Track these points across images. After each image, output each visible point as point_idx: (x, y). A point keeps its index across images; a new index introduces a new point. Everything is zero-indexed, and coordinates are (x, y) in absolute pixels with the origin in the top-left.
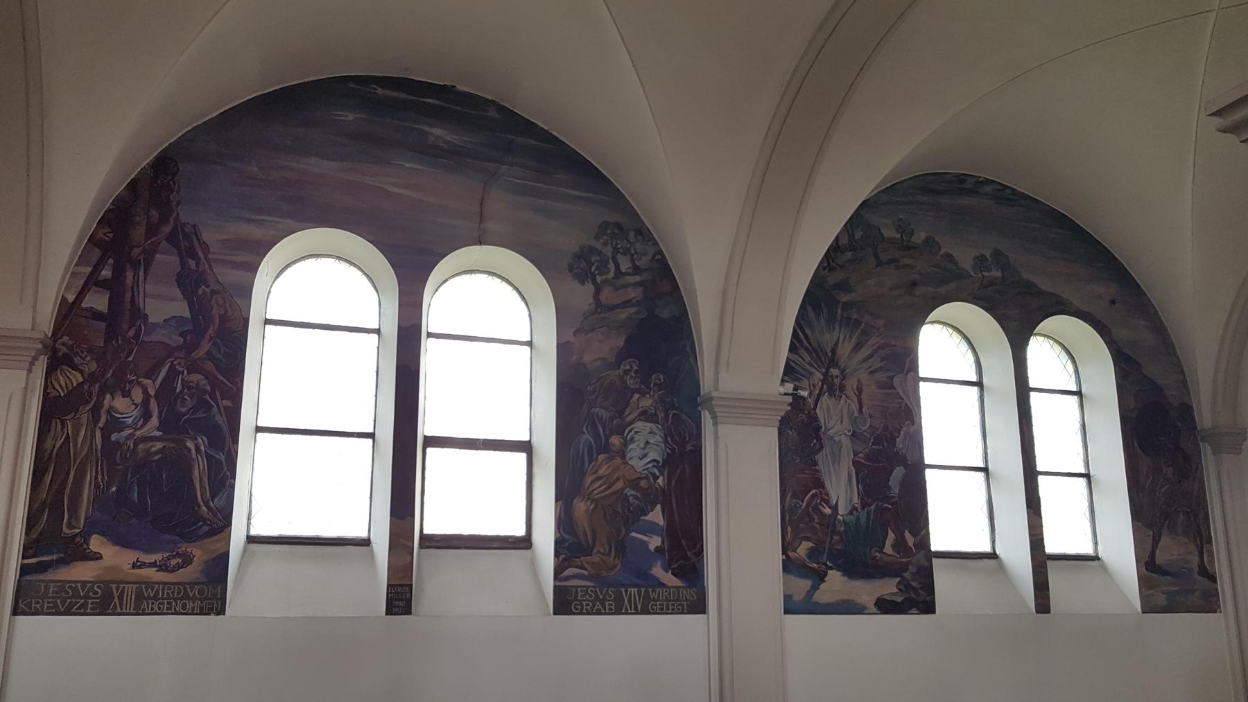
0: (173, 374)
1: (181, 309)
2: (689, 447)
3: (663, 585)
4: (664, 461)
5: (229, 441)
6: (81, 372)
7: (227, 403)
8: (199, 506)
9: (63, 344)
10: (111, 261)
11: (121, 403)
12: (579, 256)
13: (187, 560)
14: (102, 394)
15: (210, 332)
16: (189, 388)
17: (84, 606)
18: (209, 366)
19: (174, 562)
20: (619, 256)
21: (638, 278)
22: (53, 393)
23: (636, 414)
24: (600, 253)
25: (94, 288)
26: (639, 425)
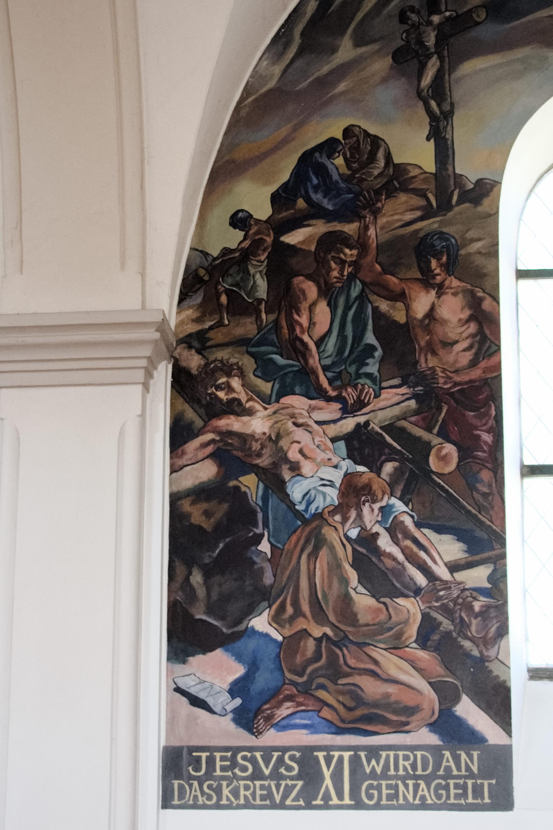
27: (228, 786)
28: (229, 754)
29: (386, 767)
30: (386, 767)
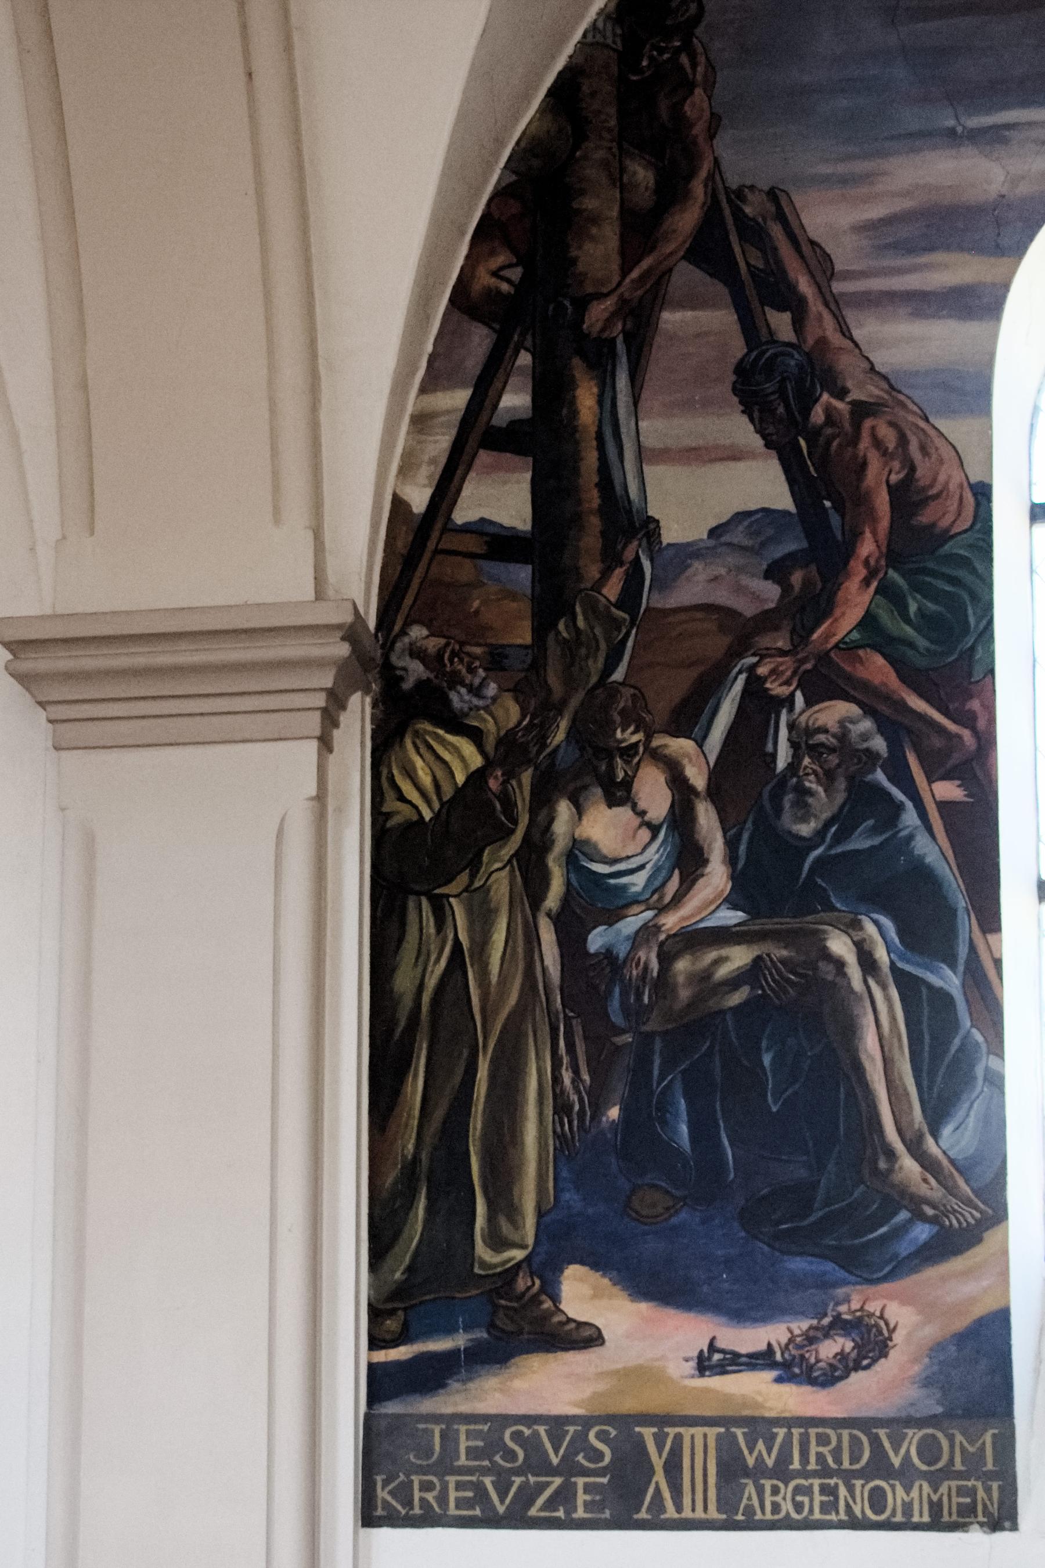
0: (759, 708)
1: (762, 484)
5: (967, 925)
6: (476, 736)
7: (948, 790)
8: (891, 1154)
9: (416, 652)
10: (525, 359)
11: (604, 827)
13: (872, 1343)
14: (542, 801)
15: (867, 547)
16: (816, 751)
17: (564, 1496)
18: (877, 668)
19: (829, 1349)
22: (403, 813)
25: (484, 457)
27: (386, 1483)
30: (784, 1458)
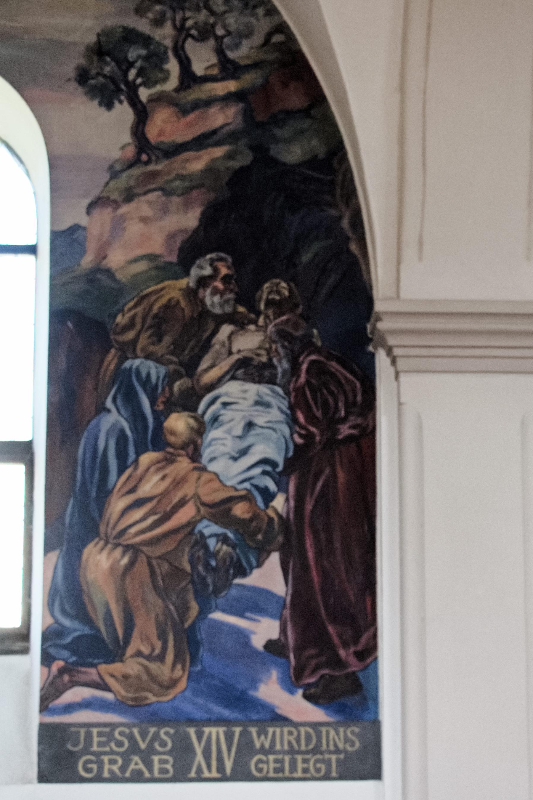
2: (345, 430)
3: (280, 720)
4: (287, 460)
12: (99, 51)
20: (189, 42)
21: (232, 86)
23: (225, 365)
24: (146, 41)
26: (232, 389)
28: (107, 730)
29: (273, 743)
30: (273, 743)
